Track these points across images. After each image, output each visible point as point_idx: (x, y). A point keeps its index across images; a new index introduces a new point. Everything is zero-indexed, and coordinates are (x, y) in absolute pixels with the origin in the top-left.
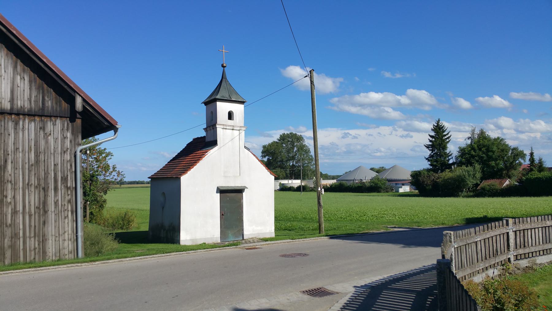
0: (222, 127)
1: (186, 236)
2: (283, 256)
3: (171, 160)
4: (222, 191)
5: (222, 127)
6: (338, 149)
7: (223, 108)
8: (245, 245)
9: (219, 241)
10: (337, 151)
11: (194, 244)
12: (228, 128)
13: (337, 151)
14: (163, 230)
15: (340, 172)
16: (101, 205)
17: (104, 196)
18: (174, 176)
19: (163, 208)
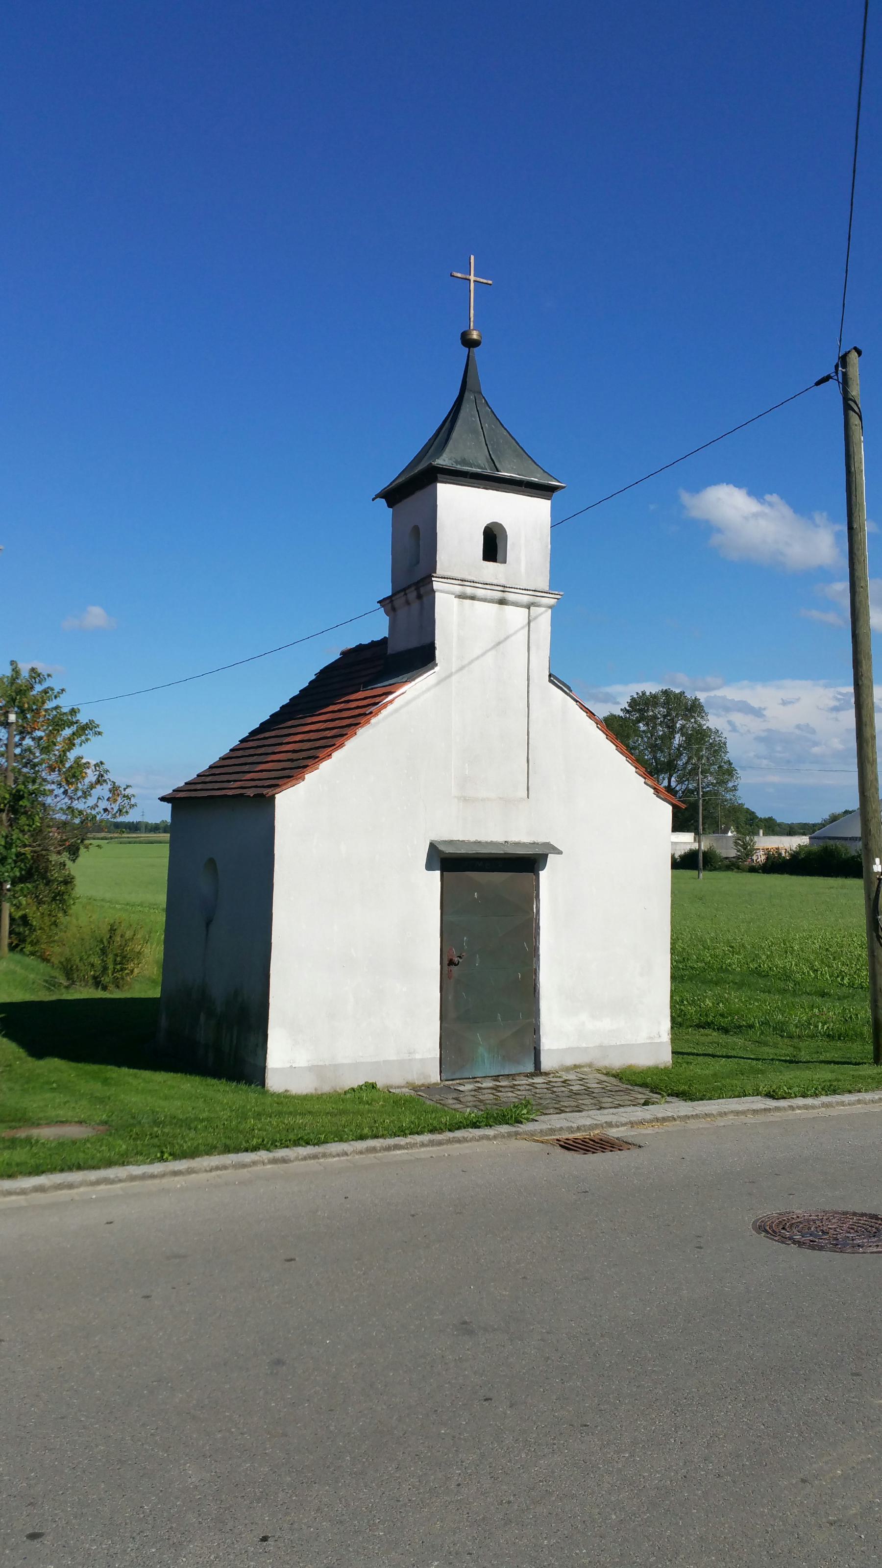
0: (458, 589)
1: (292, 1056)
2: (778, 1230)
3: (253, 733)
4: (449, 862)
5: (458, 589)
6: (816, 744)
7: (461, 511)
8: (557, 1121)
9: (434, 1076)
10: (816, 750)
11: (326, 1088)
12: (480, 593)
13: (816, 750)
14: (199, 1021)
15: (815, 817)
16: (60, 893)
17: (69, 864)
18: (251, 793)
19: (208, 923)
